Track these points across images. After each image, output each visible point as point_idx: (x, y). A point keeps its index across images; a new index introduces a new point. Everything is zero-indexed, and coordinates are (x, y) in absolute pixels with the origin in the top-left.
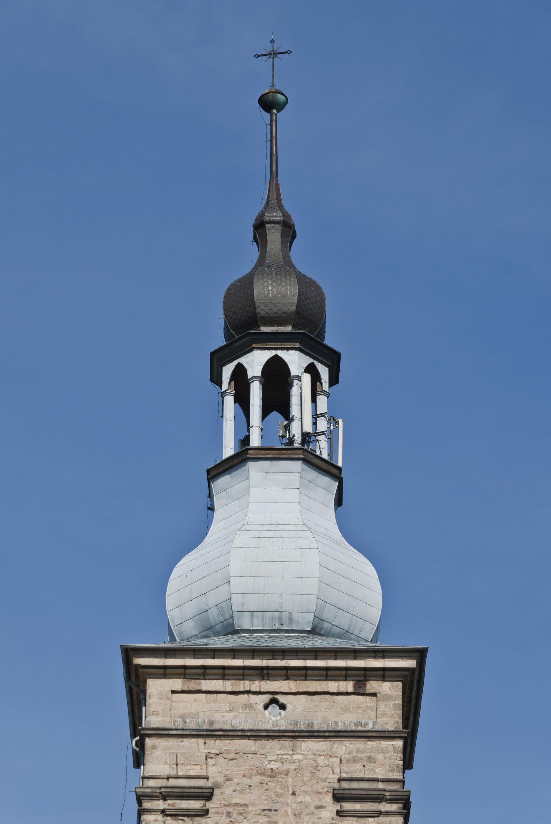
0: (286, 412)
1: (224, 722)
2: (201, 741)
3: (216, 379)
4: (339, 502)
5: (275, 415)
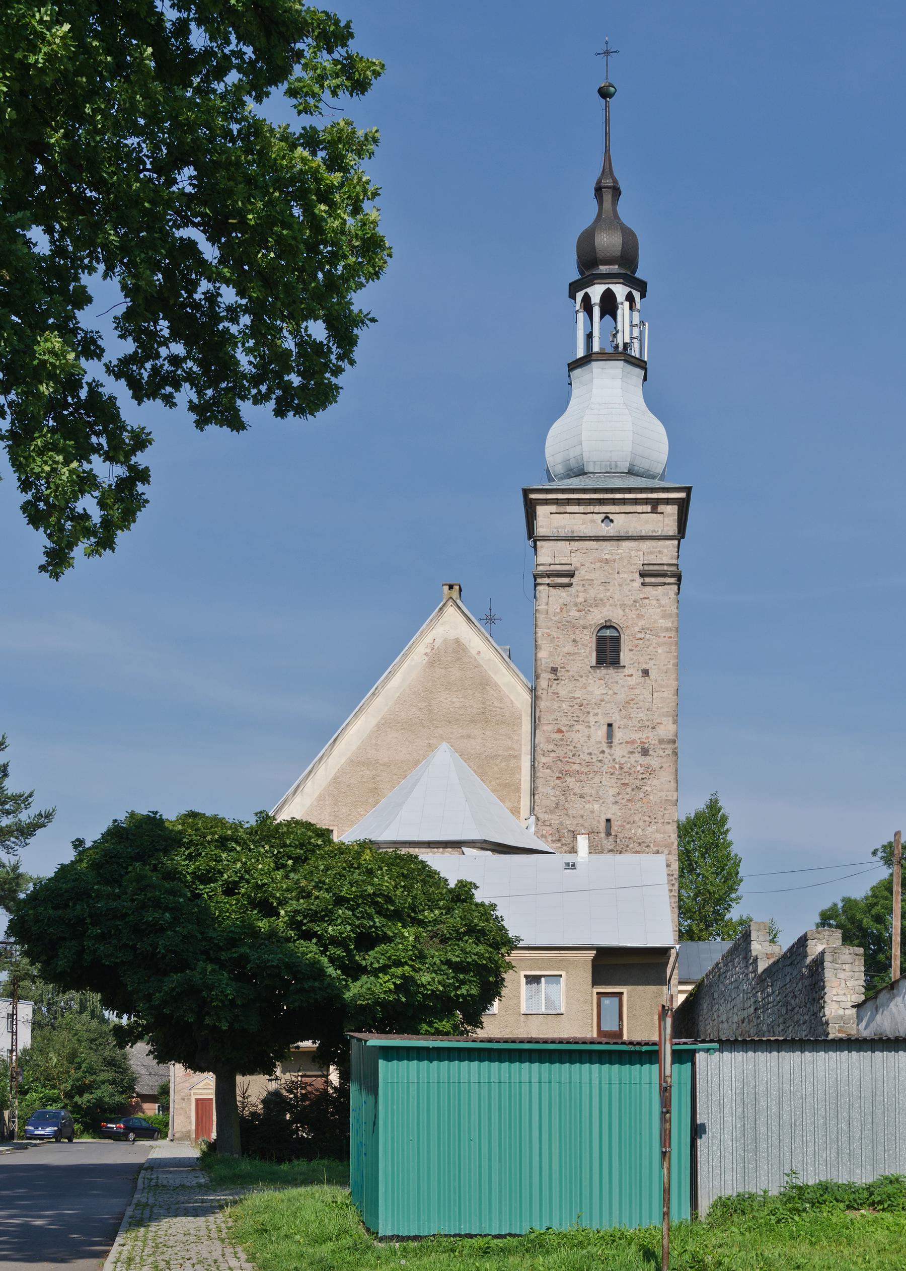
0: (614, 317)
1: (580, 531)
2: (567, 543)
3: (573, 296)
4: (645, 379)
5: (608, 317)
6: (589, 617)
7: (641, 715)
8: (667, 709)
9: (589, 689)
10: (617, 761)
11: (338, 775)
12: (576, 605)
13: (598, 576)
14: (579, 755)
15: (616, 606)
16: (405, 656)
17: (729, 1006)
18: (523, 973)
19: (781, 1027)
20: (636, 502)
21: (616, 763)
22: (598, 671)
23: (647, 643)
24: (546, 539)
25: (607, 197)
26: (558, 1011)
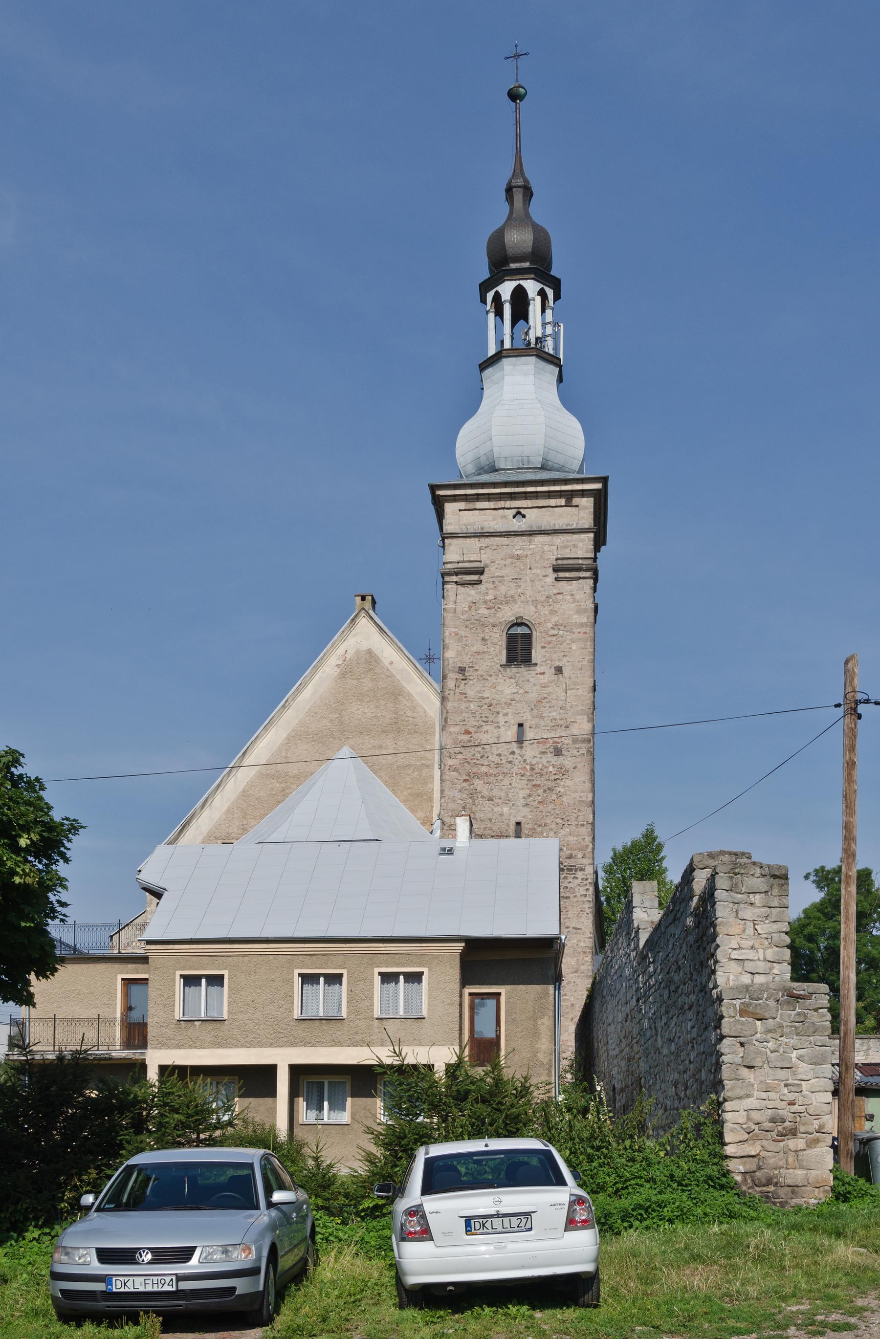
1: (490, 527)
2: (477, 539)
3: (483, 301)
4: (560, 379)
6: (499, 615)
7: (554, 714)
8: (581, 708)
9: (499, 688)
10: (528, 761)
11: (247, 788)
12: (485, 602)
13: (509, 572)
14: (488, 757)
15: (527, 602)
16: (316, 668)
17: (615, 1002)
18: (377, 970)
19: (664, 1020)
20: (549, 495)
21: (527, 764)
22: (508, 670)
23: (561, 639)
24: (454, 536)
25: (518, 196)
26: (419, 1015)
